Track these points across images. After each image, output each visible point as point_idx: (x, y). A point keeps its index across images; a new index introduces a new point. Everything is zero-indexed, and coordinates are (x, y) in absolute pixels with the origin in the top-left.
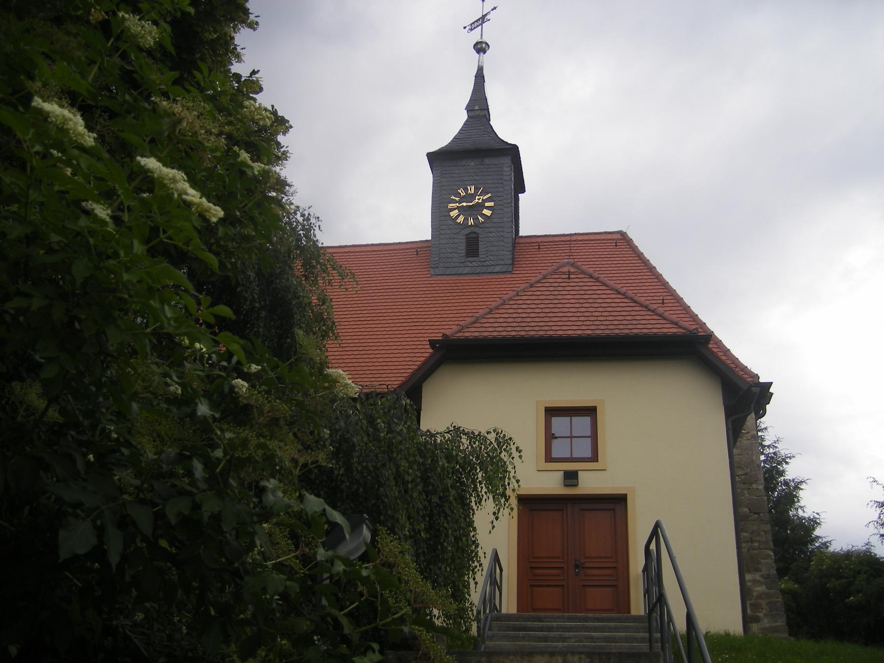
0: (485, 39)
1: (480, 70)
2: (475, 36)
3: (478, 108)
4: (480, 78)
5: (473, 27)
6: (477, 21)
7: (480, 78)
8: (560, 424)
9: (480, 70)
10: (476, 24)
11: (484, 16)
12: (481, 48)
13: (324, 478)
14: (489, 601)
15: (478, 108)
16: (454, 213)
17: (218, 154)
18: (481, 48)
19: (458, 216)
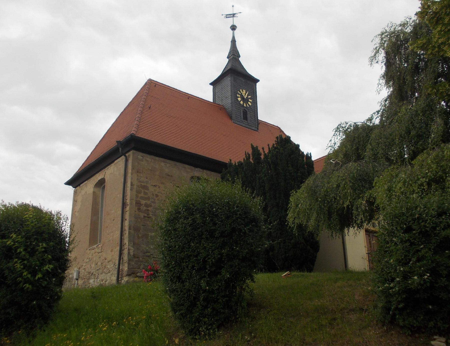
0: (235, 24)
1: (234, 37)
2: (230, 22)
3: (234, 55)
4: (234, 42)
5: (228, 16)
6: (230, 15)
7: (234, 42)
8: (256, 129)
9: (234, 37)
10: (229, 16)
11: (234, 14)
12: (233, 28)
13: (431, 324)
14: (246, 92)
15: (234, 55)
16: (250, 104)
17: (312, 240)
18: (233, 28)
19: (250, 102)
